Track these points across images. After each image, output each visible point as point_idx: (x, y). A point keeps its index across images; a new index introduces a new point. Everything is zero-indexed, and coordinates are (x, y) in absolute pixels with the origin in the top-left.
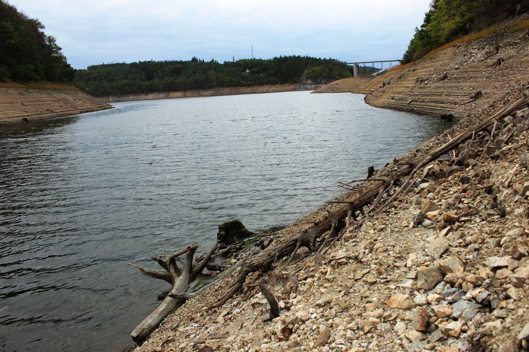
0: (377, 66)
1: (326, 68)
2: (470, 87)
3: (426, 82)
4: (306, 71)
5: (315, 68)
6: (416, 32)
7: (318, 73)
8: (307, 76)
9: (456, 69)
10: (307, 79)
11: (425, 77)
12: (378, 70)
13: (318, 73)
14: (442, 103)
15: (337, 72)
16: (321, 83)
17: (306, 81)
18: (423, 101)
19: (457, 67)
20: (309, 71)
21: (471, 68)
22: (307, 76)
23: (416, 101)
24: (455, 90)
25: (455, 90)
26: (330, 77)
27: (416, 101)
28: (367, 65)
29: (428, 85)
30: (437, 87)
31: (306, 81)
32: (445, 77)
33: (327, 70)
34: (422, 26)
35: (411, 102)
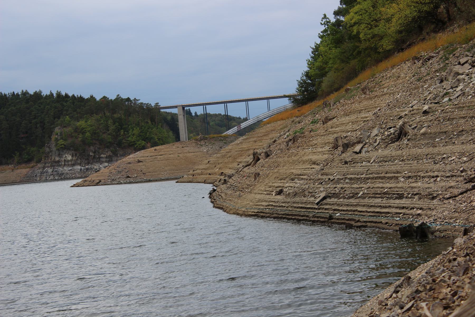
0: (236, 111)
1: (110, 122)
2: (462, 154)
3: (358, 148)
4: (57, 130)
5: (81, 123)
6: (323, 28)
7: (88, 134)
8: (61, 142)
9: (425, 112)
10: (63, 149)
11: (353, 136)
12: (239, 121)
13: (88, 134)
14: (400, 197)
15: (136, 131)
16: (99, 160)
17: (59, 155)
18: (354, 195)
19: (426, 107)
20: (66, 130)
21: (461, 108)
22: (61, 142)
23: (335, 195)
24: (427, 165)
25: (427, 165)
26: (119, 144)
27: (335, 195)
28: (212, 110)
29: (363, 154)
30: (385, 160)
31: (59, 155)
32: (401, 134)
33: (112, 128)
34: (336, 13)
35: (324, 198)
